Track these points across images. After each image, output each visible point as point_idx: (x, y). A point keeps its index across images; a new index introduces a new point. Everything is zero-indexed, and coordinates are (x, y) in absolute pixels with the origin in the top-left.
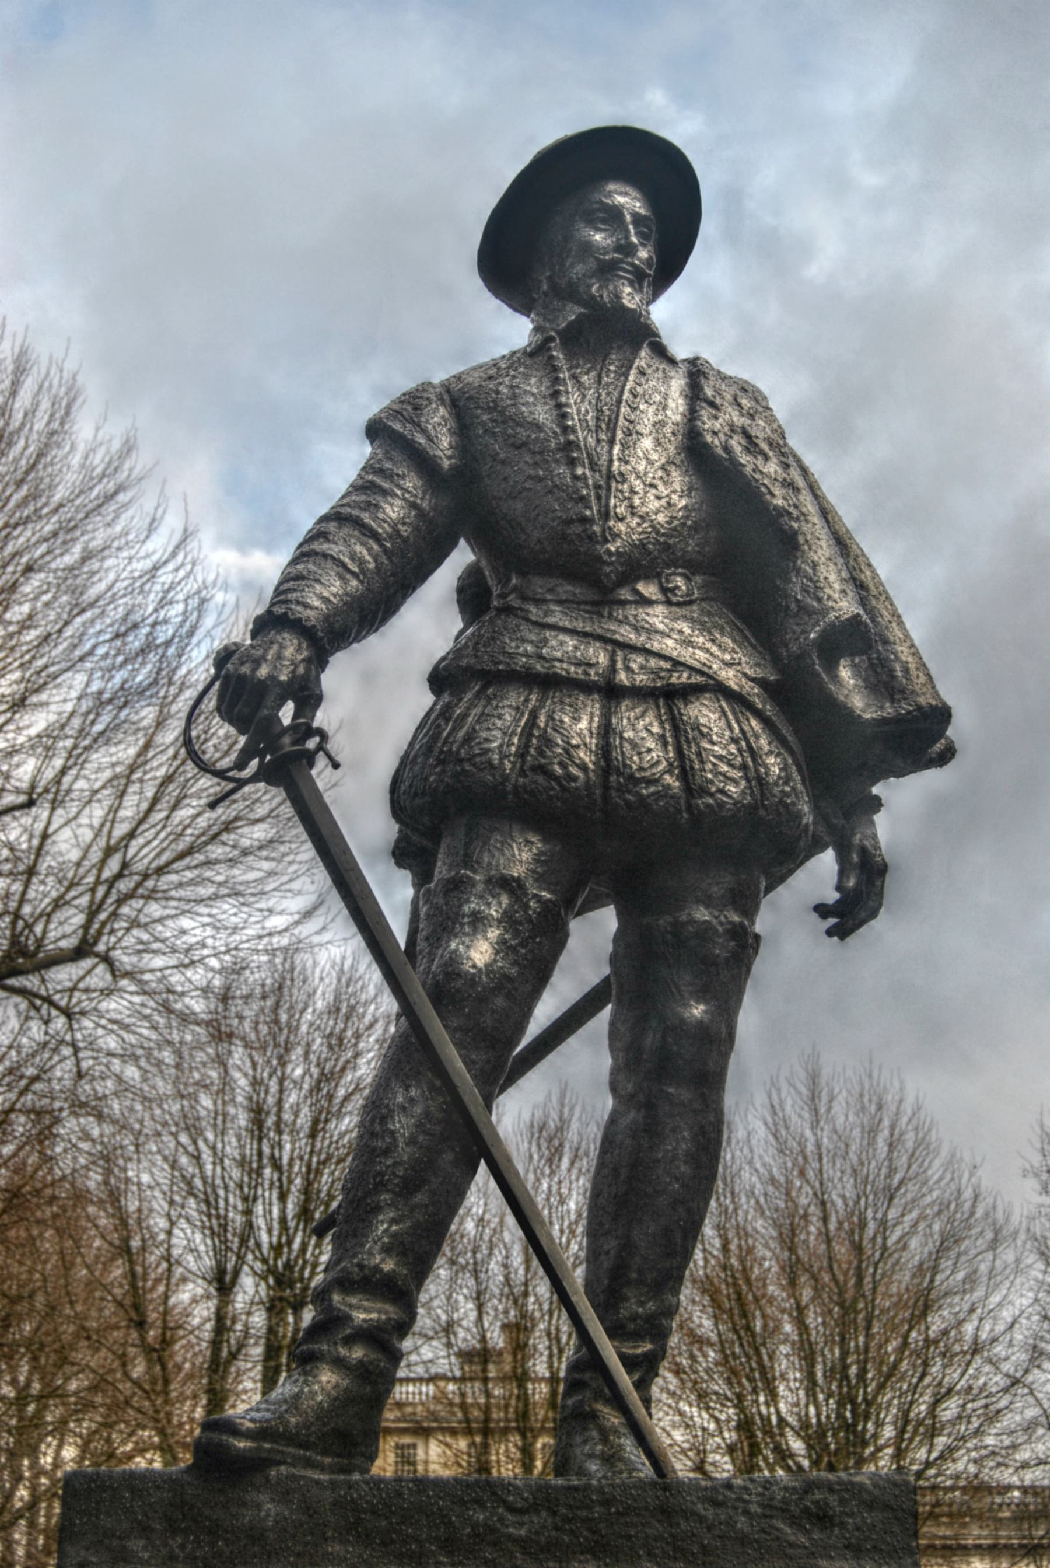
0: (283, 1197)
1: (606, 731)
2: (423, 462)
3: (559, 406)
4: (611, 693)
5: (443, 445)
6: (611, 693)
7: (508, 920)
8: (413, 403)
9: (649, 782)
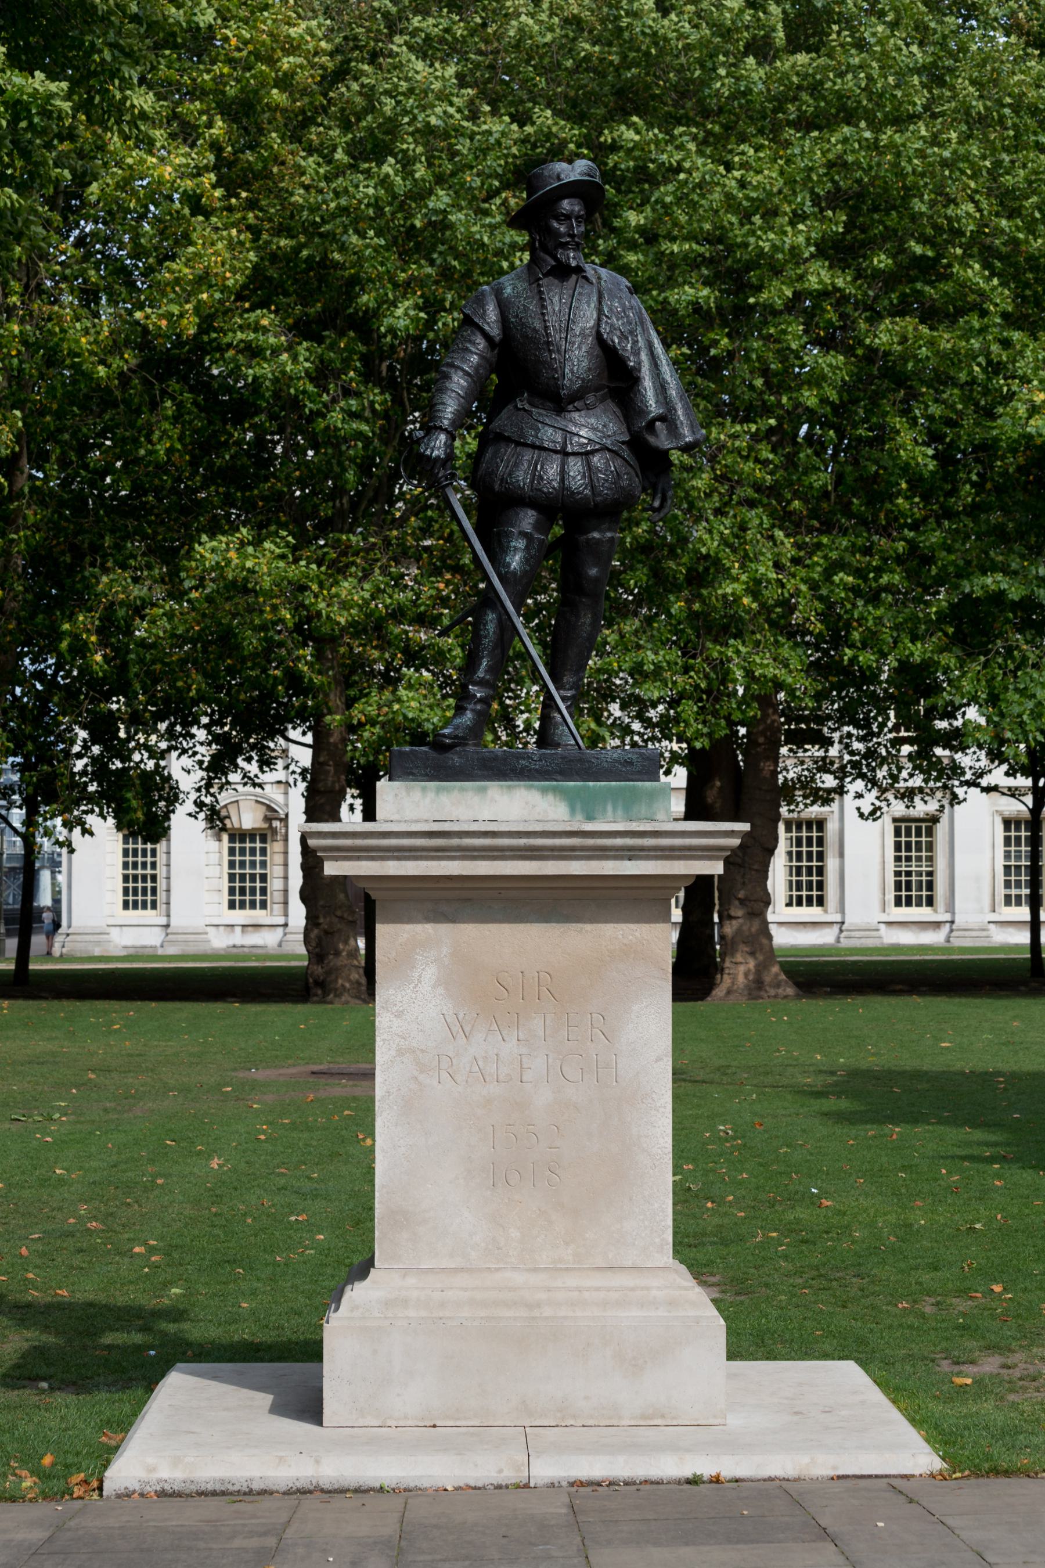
1: (563, 472)
4: (565, 454)
9: (579, 493)
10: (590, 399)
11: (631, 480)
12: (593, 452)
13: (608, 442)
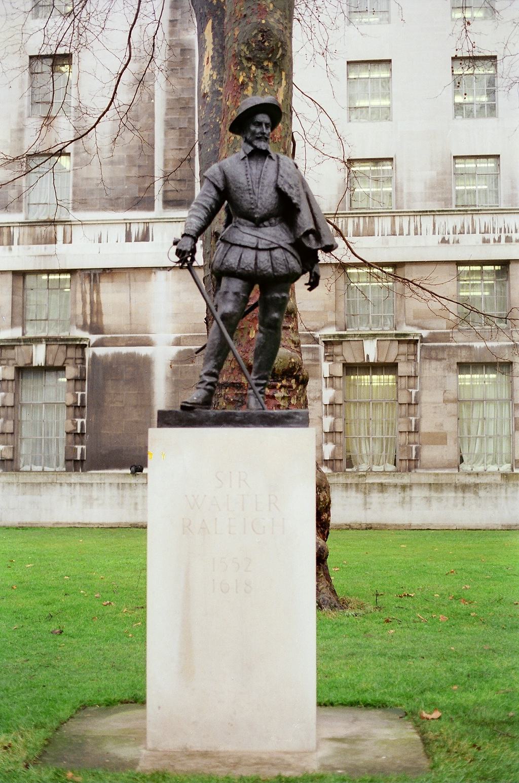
3: (247, 178)
4: (256, 249)
6: (256, 249)
10: (273, 221)
11: (294, 264)
12: (273, 249)
13: (282, 244)
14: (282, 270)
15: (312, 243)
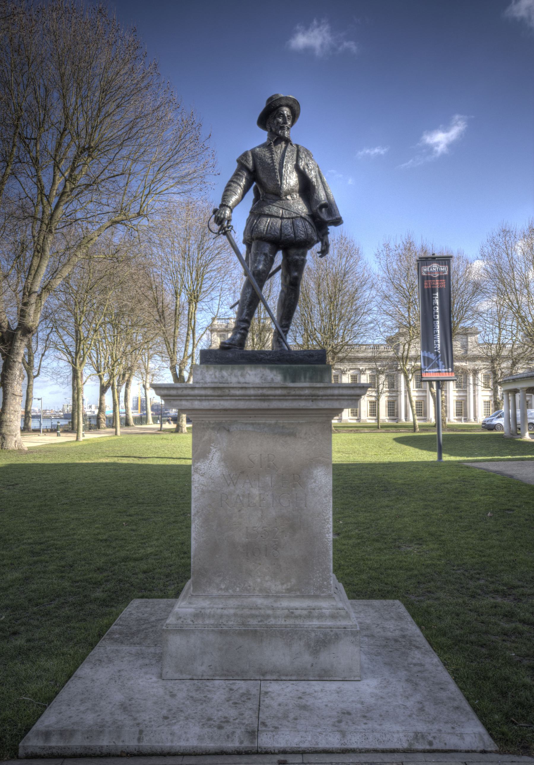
0: (191, 274)
2: (247, 169)
5: (250, 165)
7: (265, 260)
8: (245, 155)
9: (289, 235)
14: (302, 235)
15: (324, 215)
